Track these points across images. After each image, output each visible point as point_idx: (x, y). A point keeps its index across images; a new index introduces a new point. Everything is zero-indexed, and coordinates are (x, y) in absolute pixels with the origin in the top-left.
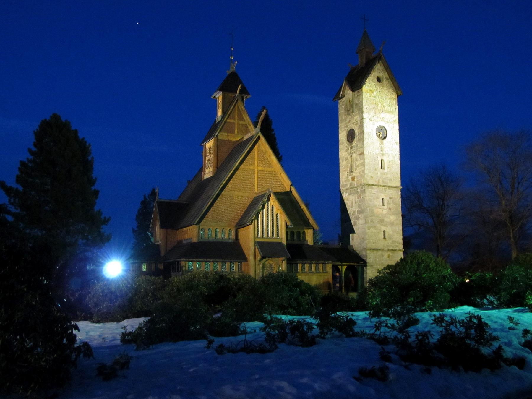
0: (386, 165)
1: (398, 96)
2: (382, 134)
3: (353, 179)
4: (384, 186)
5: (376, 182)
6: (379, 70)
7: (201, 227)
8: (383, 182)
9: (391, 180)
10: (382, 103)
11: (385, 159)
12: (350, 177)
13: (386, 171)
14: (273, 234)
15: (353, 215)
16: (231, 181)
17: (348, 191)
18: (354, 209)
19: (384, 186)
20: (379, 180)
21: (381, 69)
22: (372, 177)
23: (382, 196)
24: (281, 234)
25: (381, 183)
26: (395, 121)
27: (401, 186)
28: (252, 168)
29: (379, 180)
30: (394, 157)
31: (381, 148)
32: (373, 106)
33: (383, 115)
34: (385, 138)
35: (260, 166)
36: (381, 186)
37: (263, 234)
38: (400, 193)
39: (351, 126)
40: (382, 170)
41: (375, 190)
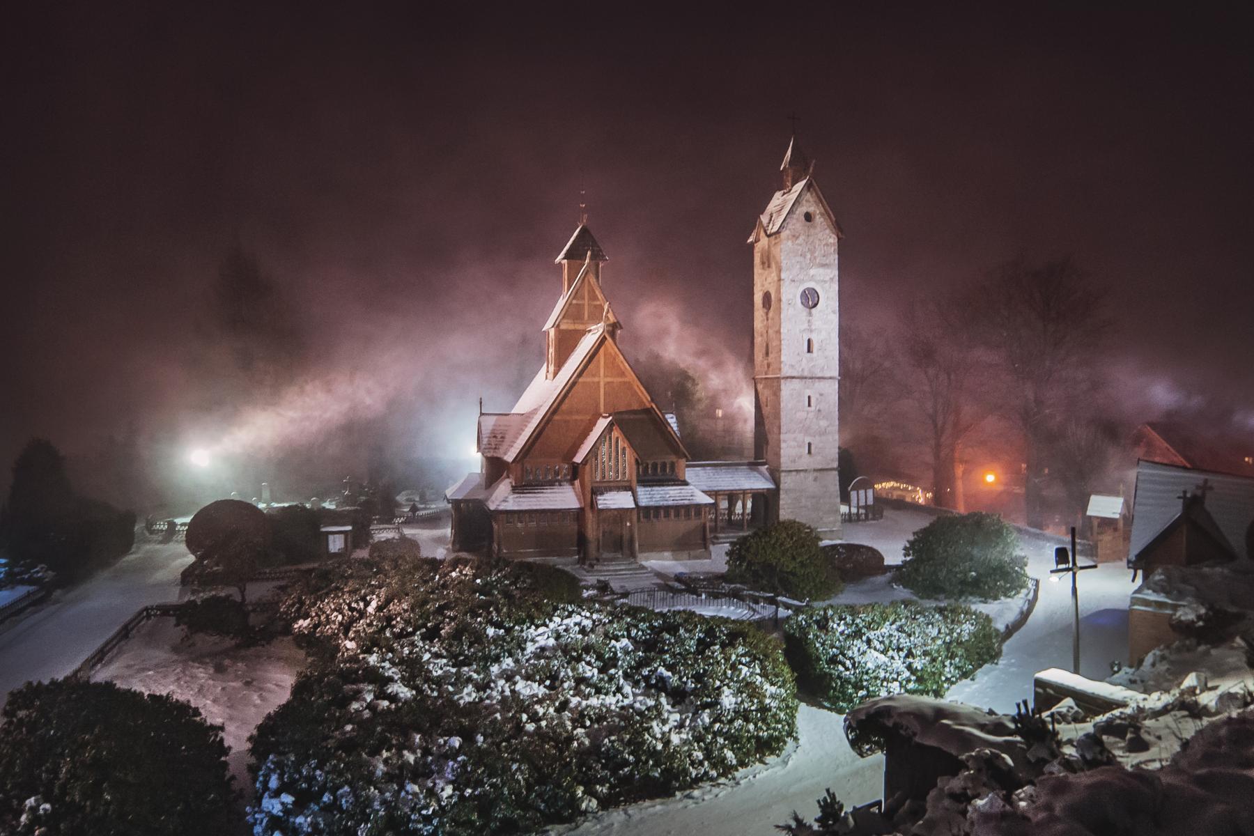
0: (815, 347)
2: (810, 299)
3: (769, 365)
10: (812, 253)
23: (808, 392)
24: (631, 475)
25: (806, 374)
28: (596, 379)
33: (812, 272)
34: (815, 305)
41: (796, 384)
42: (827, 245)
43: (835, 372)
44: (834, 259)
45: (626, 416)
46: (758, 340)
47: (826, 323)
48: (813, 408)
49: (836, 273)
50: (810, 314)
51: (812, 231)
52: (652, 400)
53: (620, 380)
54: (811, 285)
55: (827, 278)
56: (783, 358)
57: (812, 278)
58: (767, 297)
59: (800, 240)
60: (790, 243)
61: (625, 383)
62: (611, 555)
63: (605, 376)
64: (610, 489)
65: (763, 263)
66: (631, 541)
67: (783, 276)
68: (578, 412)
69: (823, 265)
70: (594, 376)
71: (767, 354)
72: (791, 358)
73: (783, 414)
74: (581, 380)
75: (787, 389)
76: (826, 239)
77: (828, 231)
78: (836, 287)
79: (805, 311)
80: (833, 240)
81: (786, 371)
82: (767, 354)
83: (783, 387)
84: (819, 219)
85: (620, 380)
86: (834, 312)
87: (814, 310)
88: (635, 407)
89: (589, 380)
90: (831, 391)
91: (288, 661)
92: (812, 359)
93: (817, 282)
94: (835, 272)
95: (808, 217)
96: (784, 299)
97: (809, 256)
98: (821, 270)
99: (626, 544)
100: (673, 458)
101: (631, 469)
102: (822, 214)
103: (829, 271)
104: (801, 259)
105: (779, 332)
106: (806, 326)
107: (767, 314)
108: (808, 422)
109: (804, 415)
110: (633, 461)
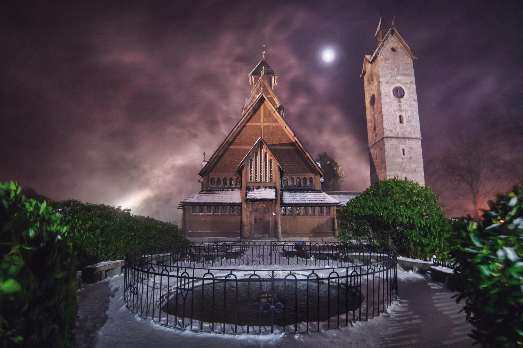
0: (405, 120)
1: (413, 62)
2: (399, 93)
3: (376, 136)
4: (403, 138)
5: (395, 134)
6: (393, 41)
7: (210, 177)
8: (402, 134)
9: (411, 132)
10: (398, 68)
11: (403, 114)
12: (374, 135)
13: (405, 124)
14: (256, 178)
15: (378, 166)
16: (238, 137)
17: (374, 147)
18: (378, 160)
19: (403, 138)
20: (398, 133)
21: (394, 40)
22: (391, 131)
23: (402, 146)
24: (276, 179)
25: (400, 136)
26: (411, 82)
27: (421, 137)
28: (258, 124)
29: (398, 133)
30: (413, 113)
31: (399, 105)
32: (390, 71)
33: (399, 78)
34: (402, 96)
35: (266, 122)
36: (400, 138)
37: (256, 178)
38: (420, 143)
39: (372, 93)
40: (400, 125)
41: (394, 141)
42: (406, 64)
43: (418, 135)
44: (412, 71)
45: (278, 147)
46: (370, 125)
47: (410, 104)
48: (406, 156)
49: (414, 79)
50: (400, 101)
51: (396, 56)
52: (295, 135)
53: (274, 124)
54: (399, 85)
55: (408, 82)
56: (385, 126)
57: (399, 81)
58: (373, 99)
59: (390, 61)
60: (383, 62)
61: (277, 127)
62: (260, 236)
63: (264, 122)
64: (259, 188)
65: (369, 81)
66: (276, 225)
67: (381, 80)
68: (246, 144)
69: (405, 75)
70: (257, 122)
71: (375, 130)
72: (390, 125)
73: (387, 159)
74: (248, 124)
75: (388, 145)
76: (407, 61)
77: (406, 57)
78: (414, 86)
79: (395, 101)
80: (410, 61)
81: (387, 133)
82: (375, 130)
83: (386, 143)
84: (400, 50)
85: (274, 124)
86: (414, 100)
87: (402, 99)
88: (284, 141)
89: (253, 124)
90: (417, 146)
91: (502, 257)
92: (403, 127)
93: (402, 84)
94: (413, 79)
95: (393, 50)
96: (382, 93)
97: (396, 70)
98: (404, 78)
99: (271, 229)
100: (312, 175)
101: (276, 174)
102: (401, 48)
103: (409, 78)
104: (392, 71)
105: (381, 112)
106: (397, 108)
107: (373, 107)
108: (404, 165)
109: (400, 160)
110: (277, 169)
